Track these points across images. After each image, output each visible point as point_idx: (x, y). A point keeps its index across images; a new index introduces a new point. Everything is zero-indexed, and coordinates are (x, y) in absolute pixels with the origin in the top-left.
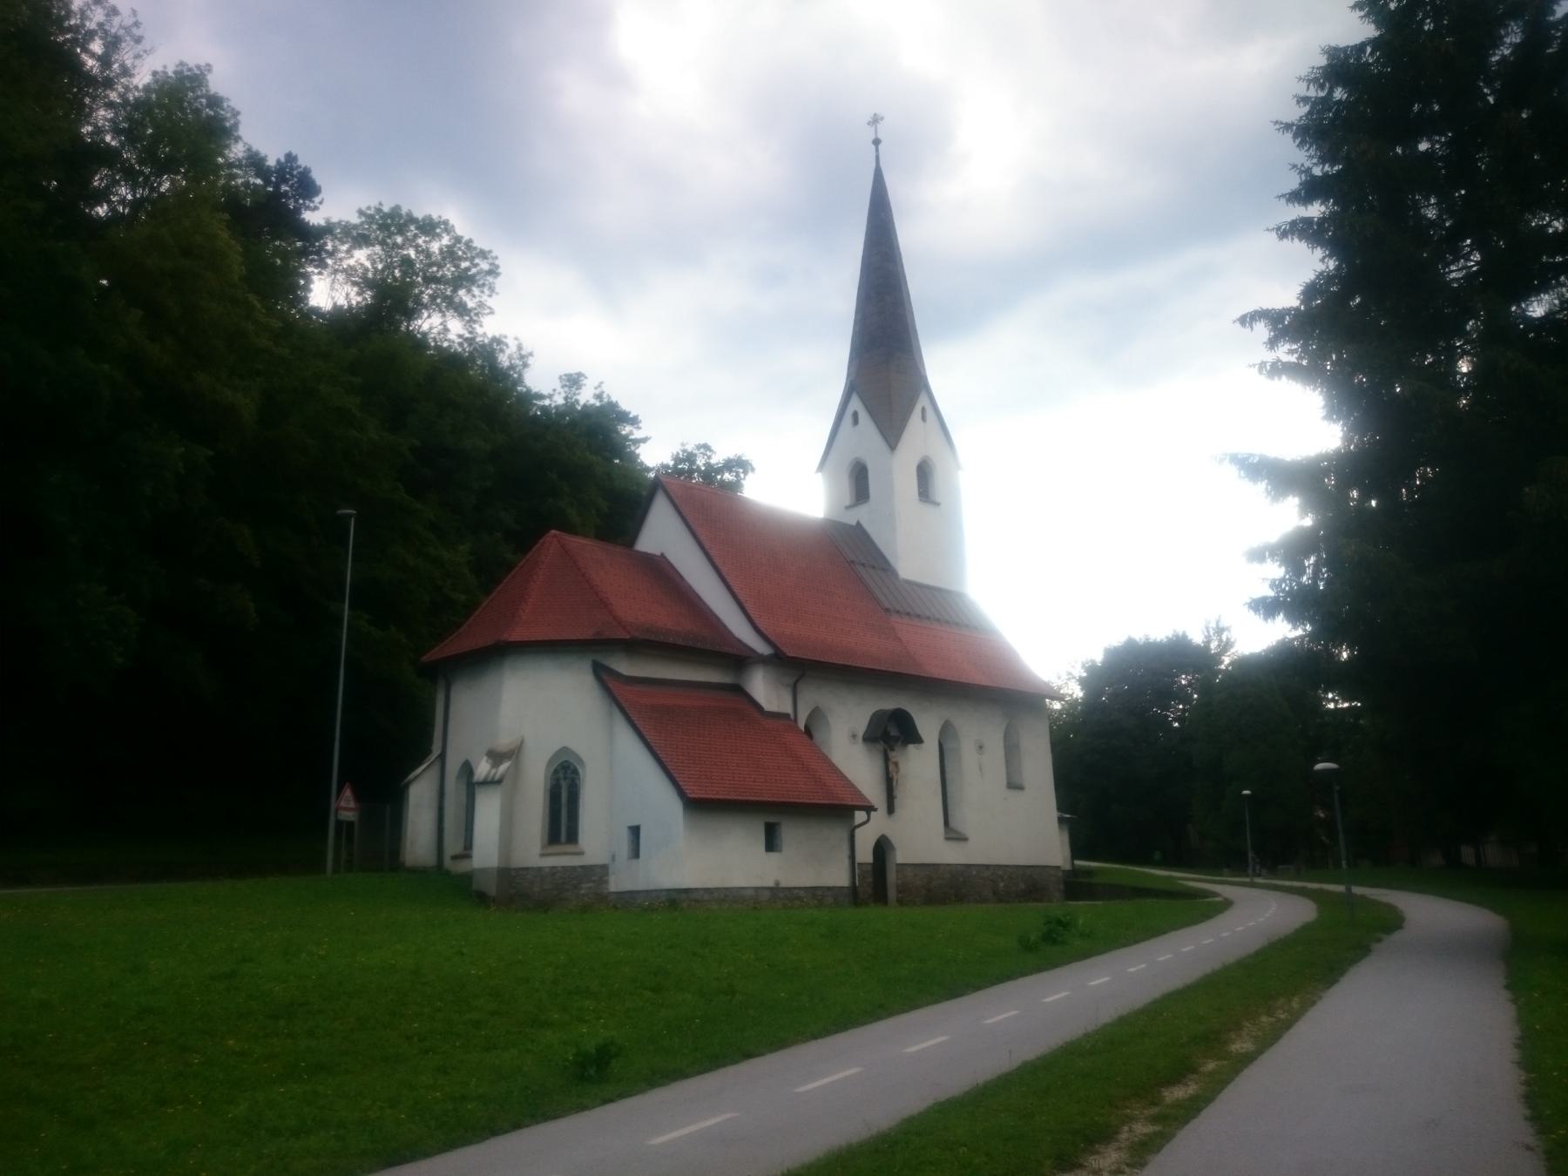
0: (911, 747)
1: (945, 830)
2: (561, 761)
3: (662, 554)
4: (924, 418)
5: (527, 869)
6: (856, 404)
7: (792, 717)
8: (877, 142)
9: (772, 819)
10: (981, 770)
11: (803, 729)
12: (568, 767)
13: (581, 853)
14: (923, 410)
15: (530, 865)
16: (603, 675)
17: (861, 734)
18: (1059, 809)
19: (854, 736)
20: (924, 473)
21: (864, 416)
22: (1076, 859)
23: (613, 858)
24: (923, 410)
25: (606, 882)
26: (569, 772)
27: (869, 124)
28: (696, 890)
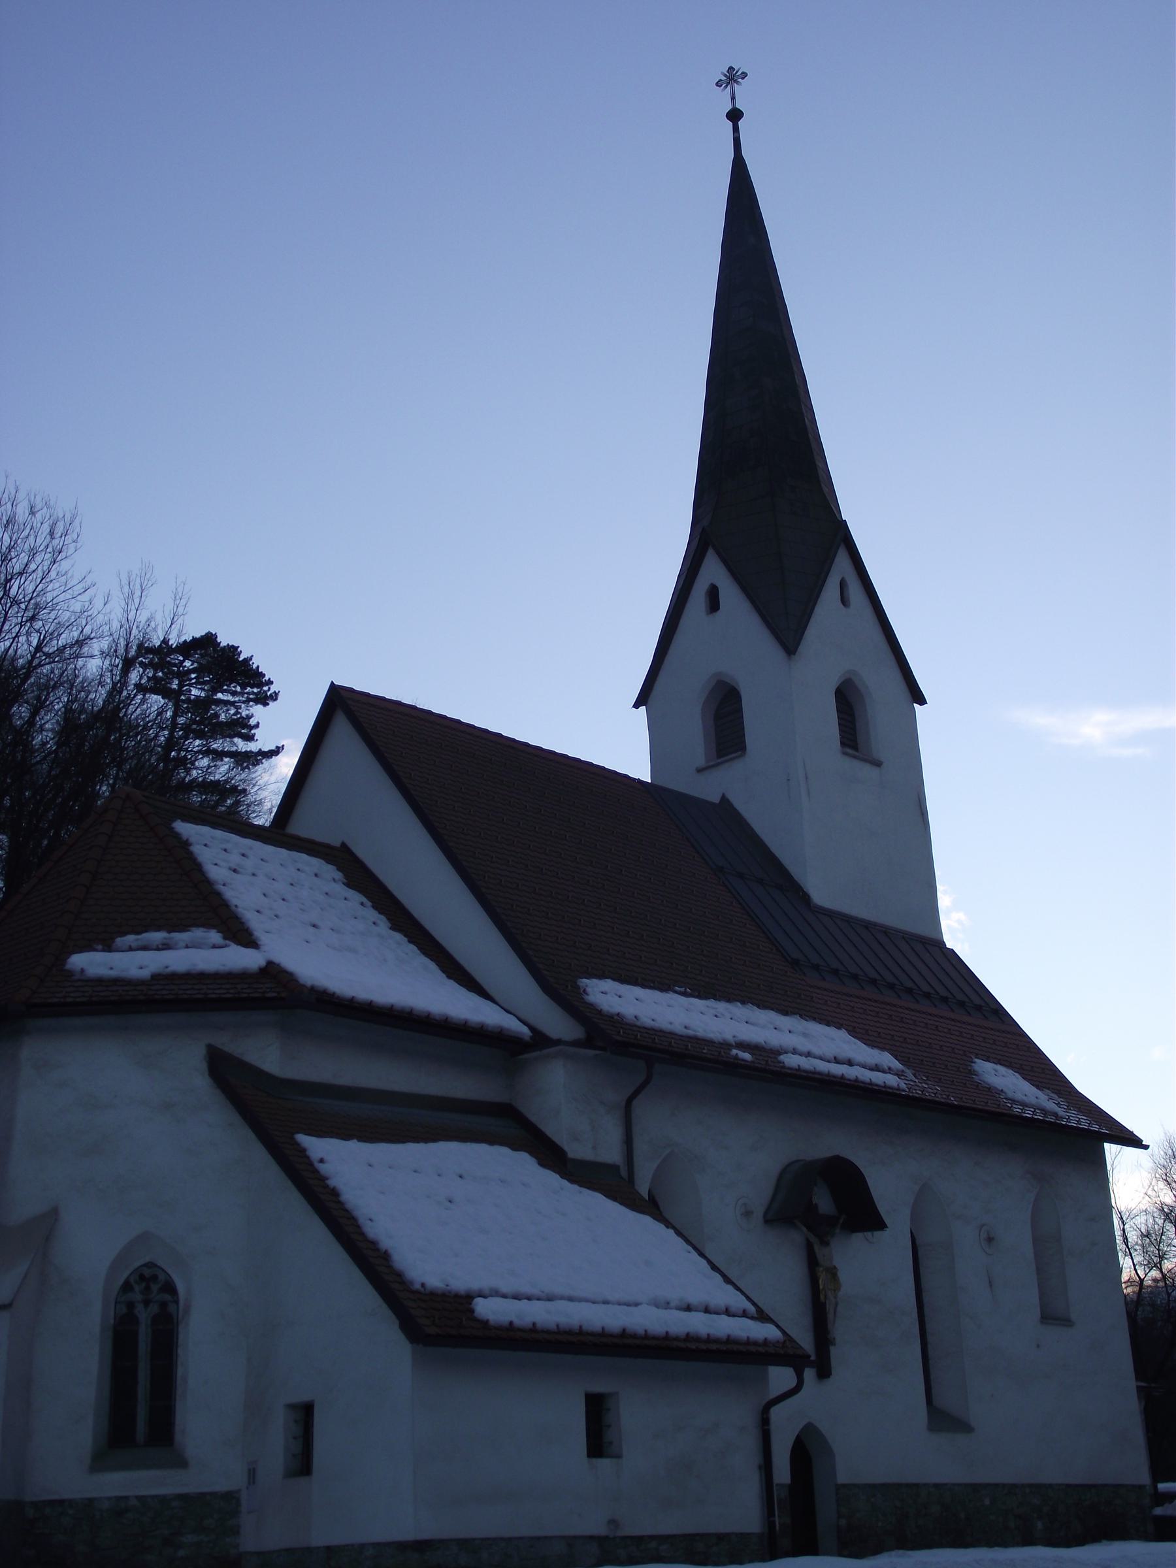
0: (858, 1238)
1: (929, 1412)
2: (137, 1264)
3: (344, 845)
4: (844, 601)
5: (61, 1502)
6: (713, 571)
7: (624, 1173)
8: (735, 116)
9: (598, 1388)
10: (991, 1284)
12: (154, 1278)
15: (66, 1495)
17: (759, 1211)
18: (1137, 1379)
19: (747, 1214)
21: (730, 594)
23: (252, 1475)
24: (843, 585)
25: (236, 1531)
26: (155, 1288)
27: (744, 75)
28: (443, 1542)
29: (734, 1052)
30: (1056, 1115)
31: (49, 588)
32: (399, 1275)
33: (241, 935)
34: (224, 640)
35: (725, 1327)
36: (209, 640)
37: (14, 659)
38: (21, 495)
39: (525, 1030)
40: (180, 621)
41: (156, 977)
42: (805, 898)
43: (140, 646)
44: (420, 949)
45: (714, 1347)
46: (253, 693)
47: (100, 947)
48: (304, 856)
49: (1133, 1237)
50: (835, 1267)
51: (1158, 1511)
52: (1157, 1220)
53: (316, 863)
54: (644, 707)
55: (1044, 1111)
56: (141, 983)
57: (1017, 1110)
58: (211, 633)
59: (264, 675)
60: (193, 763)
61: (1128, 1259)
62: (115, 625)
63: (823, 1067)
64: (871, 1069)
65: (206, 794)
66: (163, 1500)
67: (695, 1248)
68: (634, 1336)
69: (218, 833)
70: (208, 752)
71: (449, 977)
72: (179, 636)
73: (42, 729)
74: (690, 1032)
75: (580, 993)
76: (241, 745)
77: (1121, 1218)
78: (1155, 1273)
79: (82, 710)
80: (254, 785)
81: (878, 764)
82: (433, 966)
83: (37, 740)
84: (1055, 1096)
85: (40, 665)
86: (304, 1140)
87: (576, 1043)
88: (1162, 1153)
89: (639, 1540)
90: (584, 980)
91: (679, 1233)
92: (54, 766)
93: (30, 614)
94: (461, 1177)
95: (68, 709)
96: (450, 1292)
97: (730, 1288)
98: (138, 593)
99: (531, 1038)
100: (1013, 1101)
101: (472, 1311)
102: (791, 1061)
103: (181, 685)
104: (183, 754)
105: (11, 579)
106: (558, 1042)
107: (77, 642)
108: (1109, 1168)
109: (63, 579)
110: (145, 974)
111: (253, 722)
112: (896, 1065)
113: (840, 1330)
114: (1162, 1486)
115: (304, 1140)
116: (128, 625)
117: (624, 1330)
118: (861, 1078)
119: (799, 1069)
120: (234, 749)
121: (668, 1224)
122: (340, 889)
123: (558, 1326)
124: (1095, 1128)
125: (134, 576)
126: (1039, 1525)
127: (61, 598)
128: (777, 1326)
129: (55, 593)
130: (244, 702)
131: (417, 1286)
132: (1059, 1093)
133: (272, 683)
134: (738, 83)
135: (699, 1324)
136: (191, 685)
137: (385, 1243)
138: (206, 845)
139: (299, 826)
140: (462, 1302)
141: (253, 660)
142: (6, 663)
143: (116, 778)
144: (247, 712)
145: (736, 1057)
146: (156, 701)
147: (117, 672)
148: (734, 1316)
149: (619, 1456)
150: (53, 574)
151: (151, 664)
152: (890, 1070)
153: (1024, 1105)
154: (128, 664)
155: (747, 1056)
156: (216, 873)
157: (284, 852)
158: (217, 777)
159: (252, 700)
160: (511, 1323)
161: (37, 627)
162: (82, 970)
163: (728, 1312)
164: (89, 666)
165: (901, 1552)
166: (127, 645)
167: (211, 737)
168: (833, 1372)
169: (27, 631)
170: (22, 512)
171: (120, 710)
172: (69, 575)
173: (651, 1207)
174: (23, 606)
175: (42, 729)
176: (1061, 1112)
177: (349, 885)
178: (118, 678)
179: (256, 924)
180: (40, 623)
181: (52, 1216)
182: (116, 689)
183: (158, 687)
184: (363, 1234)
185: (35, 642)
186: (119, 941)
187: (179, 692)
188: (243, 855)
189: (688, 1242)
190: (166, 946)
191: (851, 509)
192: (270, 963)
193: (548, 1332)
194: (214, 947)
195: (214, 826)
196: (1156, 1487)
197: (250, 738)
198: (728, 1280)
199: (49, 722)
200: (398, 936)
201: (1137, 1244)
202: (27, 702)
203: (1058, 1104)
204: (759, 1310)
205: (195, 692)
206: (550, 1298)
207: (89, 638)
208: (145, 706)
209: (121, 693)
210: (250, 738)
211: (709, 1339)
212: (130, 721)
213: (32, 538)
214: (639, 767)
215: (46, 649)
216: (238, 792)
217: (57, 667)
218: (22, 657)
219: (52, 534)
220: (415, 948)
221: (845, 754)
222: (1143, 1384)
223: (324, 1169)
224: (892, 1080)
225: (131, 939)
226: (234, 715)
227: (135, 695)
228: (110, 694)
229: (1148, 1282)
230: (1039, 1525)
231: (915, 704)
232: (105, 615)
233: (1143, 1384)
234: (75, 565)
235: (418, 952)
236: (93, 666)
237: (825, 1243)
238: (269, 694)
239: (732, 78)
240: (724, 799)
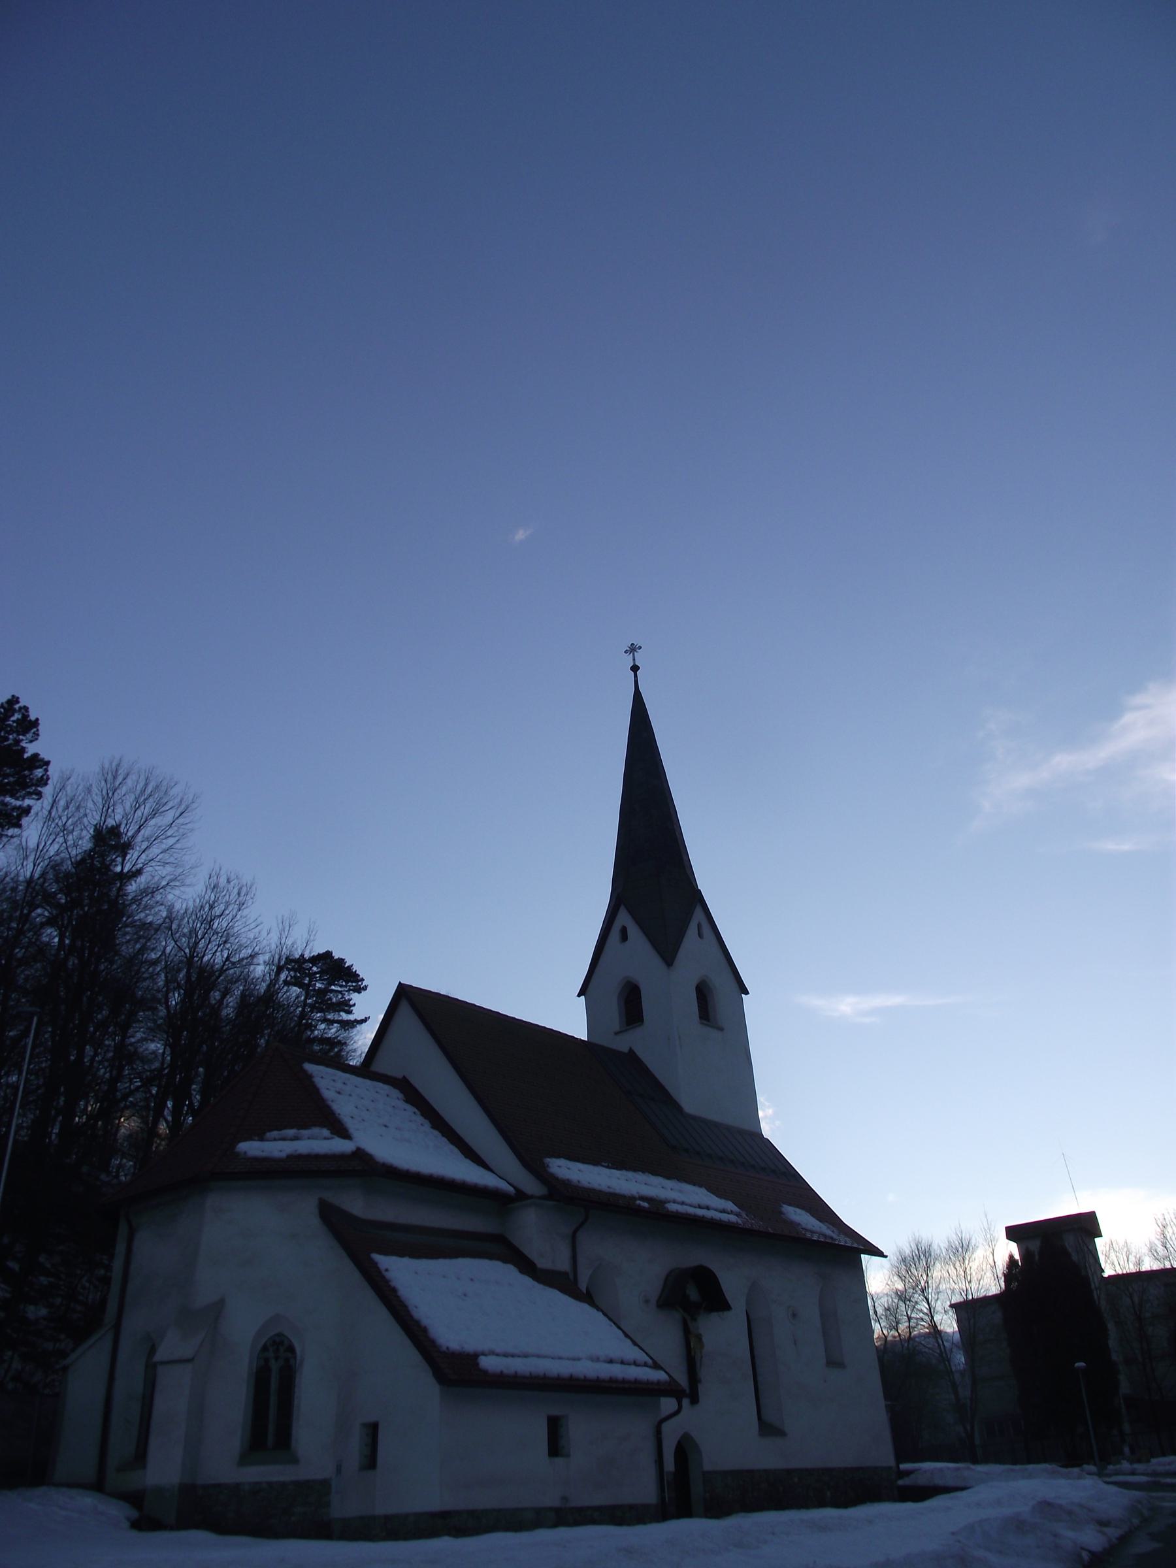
0: (714, 1315)
2: (273, 1333)
3: (404, 1077)
4: (700, 935)
5: (219, 1485)
6: (624, 918)
7: (571, 1277)
8: (635, 669)
9: (555, 1412)
11: (585, 1292)
13: (295, 1461)
14: (699, 926)
16: (331, 1217)
19: (647, 1301)
20: (703, 994)
21: (634, 931)
22: (902, 1463)
23: (339, 1469)
24: (699, 926)
27: (640, 648)
29: (638, 1202)
30: (832, 1238)
31: (236, 925)
32: (433, 1342)
33: (341, 1131)
34: (336, 955)
35: (633, 1373)
36: (328, 954)
37: (213, 966)
38: (222, 872)
39: (511, 1189)
40: (311, 944)
41: (289, 1157)
42: (678, 1108)
43: (287, 958)
44: (449, 1140)
45: (627, 1386)
46: (352, 986)
47: (256, 1138)
48: (381, 1084)
49: (880, 1310)
50: (701, 1335)
51: (900, 1482)
52: (894, 1300)
53: (384, 1088)
54: (583, 997)
55: (825, 1236)
56: (280, 1160)
57: (808, 1235)
58: (329, 952)
59: (359, 976)
60: (315, 1027)
61: (878, 1324)
62: (273, 946)
63: (691, 1210)
64: (721, 1212)
65: (323, 1045)
66: (283, 1485)
67: (615, 1323)
68: (578, 1379)
69: (329, 1070)
70: (325, 1020)
71: (466, 1157)
72: (310, 953)
73: (227, 1006)
74: (611, 1191)
75: (545, 1167)
76: (344, 1016)
77: (873, 1299)
78: (894, 1333)
79: (251, 995)
80: (352, 1040)
81: (721, 1029)
82: (456, 1150)
83: (224, 1012)
84: (831, 1226)
85: (228, 969)
86: (377, 1257)
87: (541, 1198)
88: (896, 1259)
89: (580, 1510)
90: (548, 1159)
91: (605, 1314)
92: (141, 1089)
93: (224, 939)
94: (472, 1280)
95: (243, 995)
96: (464, 1352)
97: (636, 1348)
98: (287, 928)
99: (515, 1194)
100: (806, 1230)
101: (478, 1364)
102: (673, 1207)
103: (310, 981)
104: (310, 1021)
105: (214, 920)
106: (532, 1197)
107: (250, 956)
108: (864, 1268)
109: (244, 920)
110: (283, 1155)
111: (352, 1003)
112: (735, 1209)
113: (706, 1374)
114: (903, 1466)
115: (377, 1257)
116: (280, 946)
117: (571, 1375)
118: (714, 1217)
119: (677, 1212)
120: (340, 1018)
121: (598, 1309)
122: (402, 1104)
123: (531, 1374)
124: (855, 1245)
125: (285, 918)
126: (829, 1494)
127: (242, 930)
128: (666, 1372)
129: (239, 928)
130: (347, 991)
131: (444, 1348)
132: (834, 1225)
133: (364, 980)
134: (637, 652)
135: (617, 1371)
136: (316, 981)
137: (425, 1322)
138: (322, 1077)
139: (379, 1066)
140: (469, 1360)
141: (353, 966)
142: (208, 968)
143: (269, 1035)
144: (349, 997)
145: (639, 1205)
146: (296, 990)
147: (273, 974)
148: (639, 1365)
149: (568, 1456)
150: (238, 917)
151: (293, 969)
152: (732, 1212)
153: (813, 1232)
154: (280, 969)
155: (646, 1205)
156: (328, 1094)
157: (368, 1082)
158: (330, 1035)
159: (351, 990)
160: (502, 1372)
161: (227, 947)
162: (245, 1153)
163: (635, 1364)
164: (257, 970)
165: (743, 1514)
166: (280, 958)
167: (327, 1012)
168: (700, 1400)
169: (221, 950)
170: (223, 881)
171: (273, 996)
172: (248, 916)
173: (587, 1298)
174: (220, 935)
175: (227, 1006)
176: (835, 1236)
177: (407, 1101)
178: (274, 977)
179: (351, 1125)
180: (229, 945)
181: (220, 1304)
182: (273, 983)
183: (297, 983)
184: (411, 1316)
185: (225, 956)
186: (268, 1135)
187: (309, 985)
188: (344, 1083)
189: (610, 1319)
190: (296, 1138)
191: (704, 883)
192: (358, 1149)
193: (524, 1377)
194: (326, 1138)
195: (327, 1066)
196: (898, 1467)
197: (350, 1012)
198: (635, 1343)
199: (232, 1000)
200: (436, 1133)
201: (882, 1315)
202: (219, 991)
203: (833, 1231)
204: (655, 1363)
205: (318, 985)
206: (526, 1356)
207: (257, 954)
208: (288, 994)
209: (275, 985)
210: (350, 1012)
211: (624, 1381)
212: (279, 1002)
213: (227, 896)
214: (580, 1032)
215: (233, 960)
216: (342, 1044)
217: (238, 971)
218: (217, 964)
219: (239, 894)
220: (446, 1140)
221: (702, 1023)
222: (889, 1403)
223: (388, 1275)
224: (733, 1218)
225: (275, 1133)
226: (341, 998)
227: (283, 987)
228: (269, 986)
229: (889, 1338)
230: (829, 1494)
231: (743, 995)
232: (267, 940)
233: (889, 1403)
234: (251, 912)
235: (448, 1142)
236: (259, 970)
237: (694, 1319)
238: (362, 986)
239: (633, 649)
240: (631, 1050)
